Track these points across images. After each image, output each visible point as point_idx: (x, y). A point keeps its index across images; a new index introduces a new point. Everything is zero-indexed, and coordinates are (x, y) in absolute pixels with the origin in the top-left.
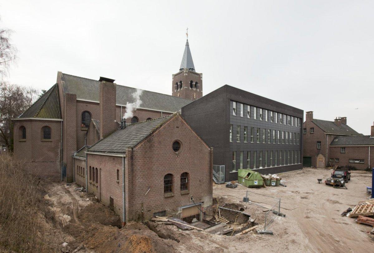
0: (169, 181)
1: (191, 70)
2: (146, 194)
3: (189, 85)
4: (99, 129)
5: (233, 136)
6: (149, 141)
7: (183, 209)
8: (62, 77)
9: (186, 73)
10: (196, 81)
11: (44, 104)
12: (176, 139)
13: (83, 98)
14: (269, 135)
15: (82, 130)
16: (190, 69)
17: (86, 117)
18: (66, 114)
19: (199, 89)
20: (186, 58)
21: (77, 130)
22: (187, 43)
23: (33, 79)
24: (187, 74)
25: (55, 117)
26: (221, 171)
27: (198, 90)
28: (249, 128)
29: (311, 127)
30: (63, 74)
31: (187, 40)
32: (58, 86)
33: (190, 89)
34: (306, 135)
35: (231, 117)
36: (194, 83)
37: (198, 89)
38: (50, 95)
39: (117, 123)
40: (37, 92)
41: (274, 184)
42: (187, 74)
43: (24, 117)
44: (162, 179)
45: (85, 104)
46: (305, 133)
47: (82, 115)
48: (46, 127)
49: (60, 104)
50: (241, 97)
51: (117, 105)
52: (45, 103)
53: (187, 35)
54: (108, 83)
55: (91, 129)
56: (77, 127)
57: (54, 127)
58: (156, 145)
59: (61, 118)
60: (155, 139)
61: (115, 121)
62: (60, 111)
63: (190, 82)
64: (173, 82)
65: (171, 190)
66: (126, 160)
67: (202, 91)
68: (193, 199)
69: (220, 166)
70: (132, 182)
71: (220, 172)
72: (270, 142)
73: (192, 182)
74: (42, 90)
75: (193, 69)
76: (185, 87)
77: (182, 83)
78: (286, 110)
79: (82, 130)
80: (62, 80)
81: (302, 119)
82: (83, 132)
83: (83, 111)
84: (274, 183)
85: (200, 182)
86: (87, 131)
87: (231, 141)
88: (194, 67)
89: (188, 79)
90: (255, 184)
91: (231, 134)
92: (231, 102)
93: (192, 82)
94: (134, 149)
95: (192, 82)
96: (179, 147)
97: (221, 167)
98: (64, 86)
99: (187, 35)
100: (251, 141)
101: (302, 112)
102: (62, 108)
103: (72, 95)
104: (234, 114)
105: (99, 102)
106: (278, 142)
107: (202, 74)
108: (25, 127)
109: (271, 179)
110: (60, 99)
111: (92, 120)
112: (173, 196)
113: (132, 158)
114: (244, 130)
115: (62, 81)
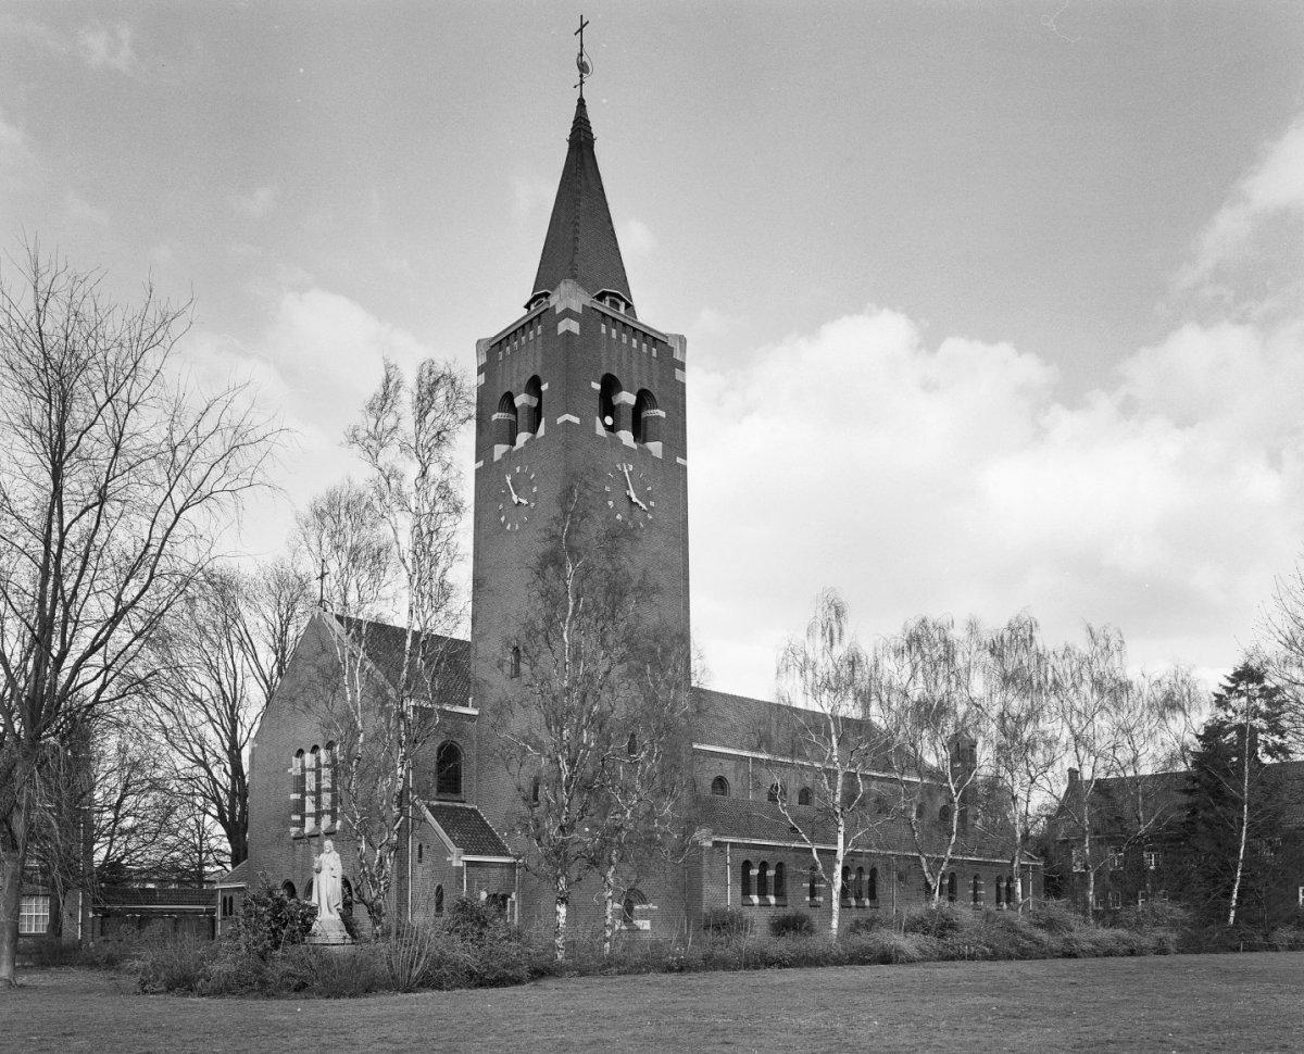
3: (595, 404)
63: (597, 386)
77: (544, 387)
93: (610, 385)
95: (610, 385)
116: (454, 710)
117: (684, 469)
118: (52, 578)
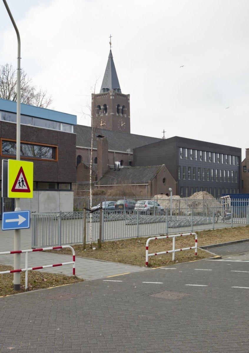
9: (113, 95)
10: (123, 105)
14: (208, 173)
19: (126, 115)
22: (111, 54)
27: (125, 116)
28: (192, 168)
31: (111, 50)
33: (117, 115)
35: (179, 160)
37: (126, 114)
42: (114, 98)
50: (186, 144)
51: (109, 150)
53: (111, 44)
63: (116, 107)
67: (130, 116)
72: (200, 179)
75: (119, 90)
76: (112, 113)
78: (223, 150)
81: (240, 157)
88: (120, 88)
99: (111, 44)
100: (184, 178)
101: (239, 150)
105: (96, 149)
106: (229, 180)
107: (129, 95)
113: (151, 185)
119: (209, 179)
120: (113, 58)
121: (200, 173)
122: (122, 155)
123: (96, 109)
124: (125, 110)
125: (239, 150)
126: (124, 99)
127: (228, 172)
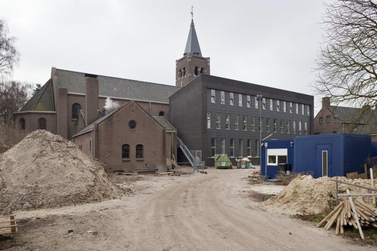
0: (126, 150)
1: (196, 55)
2: (107, 156)
3: (194, 72)
4: (85, 118)
5: (211, 123)
6: (110, 120)
7: (138, 172)
8: (56, 72)
9: (189, 58)
10: (202, 67)
11: (40, 98)
12: (131, 119)
13: (74, 91)
15: (72, 121)
16: (195, 53)
17: (76, 108)
18: (58, 107)
20: (191, 41)
21: (68, 121)
22: (192, 23)
23: (30, 75)
24: (190, 60)
25: (45, 109)
26: (197, 156)
29: (327, 115)
30: (56, 69)
31: (192, 20)
32: (52, 80)
33: (195, 76)
34: (323, 125)
36: (199, 69)
38: (45, 90)
39: (99, 112)
40: (31, 86)
41: (244, 166)
42: (190, 60)
43: (23, 111)
44: (121, 147)
45: (75, 97)
46: (322, 122)
47: (73, 107)
48: (42, 118)
49: (54, 98)
50: (220, 84)
51: (99, 96)
52: (41, 97)
53: (192, 14)
54: (92, 78)
55: (80, 119)
56: (68, 118)
57: (47, 118)
58: (115, 123)
59: (55, 110)
60: (115, 119)
61: (98, 110)
62: (54, 104)
63: (194, 69)
64: (177, 69)
65: (128, 157)
66: (94, 132)
68: (147, 166)
69: (196, 151)
70: (98, 147)
71: (196, 157)
73: (146, 151)
74: (36, 85)
75: (199, 53)
76: (189, 75)
77: (186, 69)
78: (285, 96)
79: (72, 121)
80: (56, 76)
81: (312, 107)
82: (74, 122)
83: (73, 103)
84: (244, 166)
85: (154, 153)
86: (77, 121)
87: (209, 127)
89: (193, 64)
90: (223, 165)
91: (209, 121)
92: (208, 90)
93: (196, 68)
94: (99, 125)
95: (196, 68)
96: (136, 125)
97: (197, 152)
98: (57, 81)
99: (192, 14)
101: (311, 98)
102: (56, 101)
103: (64, 89)
104: (213, 101)
105: (84, 94)
107: (209, 58)
108: (25, 119)
109: (240, 162)
110: (54, 93)
111: (80, 111)
112: (129, 161)
114: (242, 119)
115: (55, 77)
116: (295, 126)
117: (209, 66)
118: (209, 121)
119: (284, 131)
120: (195, 27)
121: (290, 125)
122: (162, 106)
123: (179, 73)
124: (205, 71)
125: (311, 98)
126: (203, 62)
127: (299, 124)
